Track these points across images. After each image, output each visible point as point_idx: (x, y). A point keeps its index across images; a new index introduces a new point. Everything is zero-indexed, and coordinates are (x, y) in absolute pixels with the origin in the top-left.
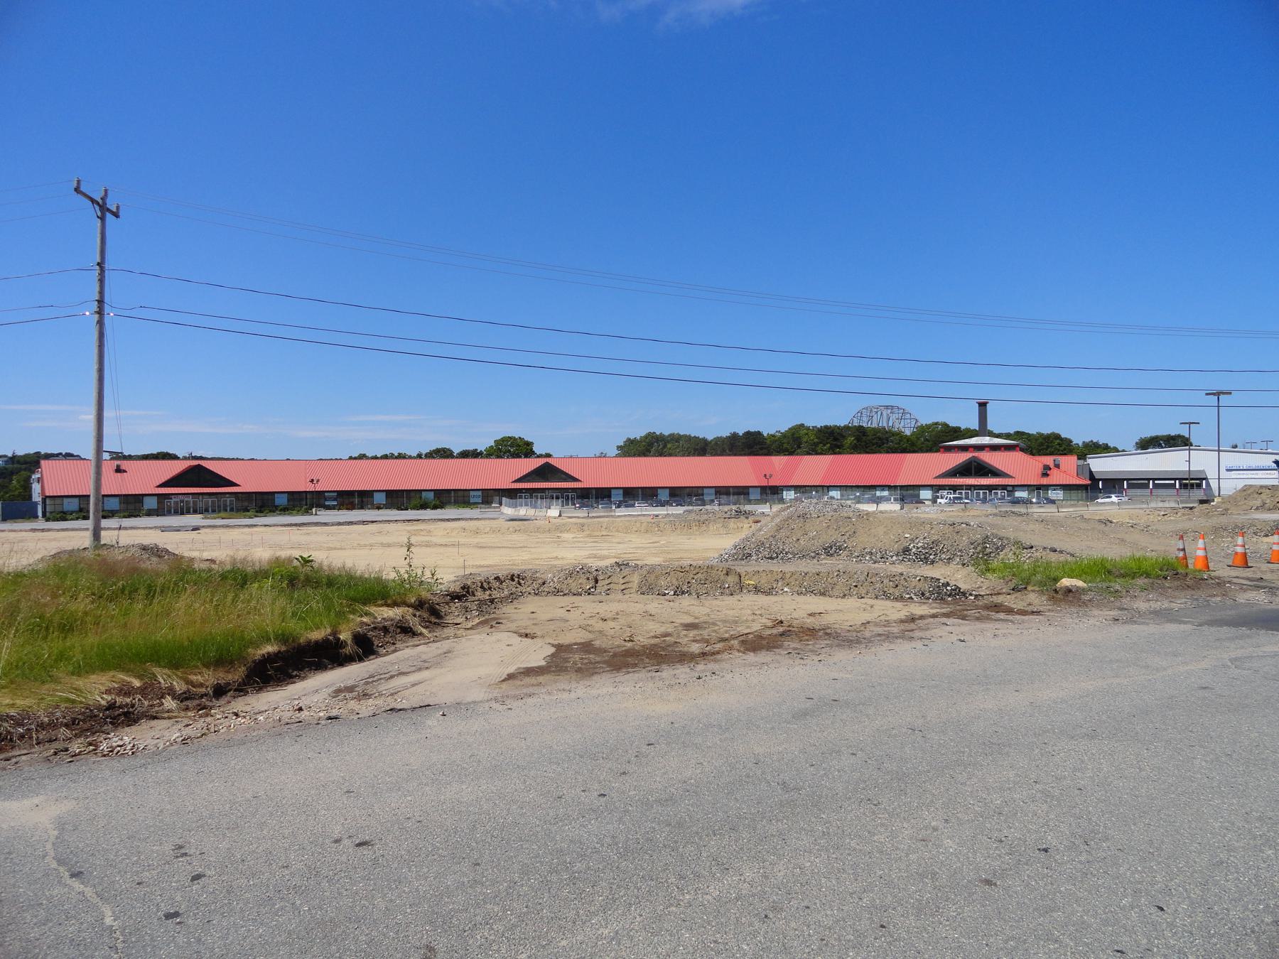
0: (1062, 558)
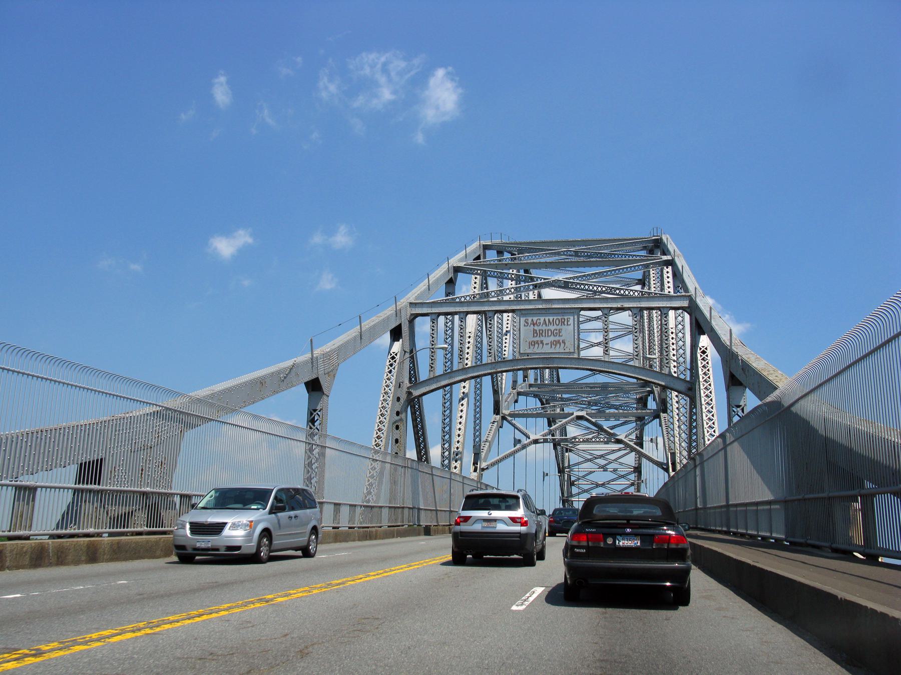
0: (666, 242)
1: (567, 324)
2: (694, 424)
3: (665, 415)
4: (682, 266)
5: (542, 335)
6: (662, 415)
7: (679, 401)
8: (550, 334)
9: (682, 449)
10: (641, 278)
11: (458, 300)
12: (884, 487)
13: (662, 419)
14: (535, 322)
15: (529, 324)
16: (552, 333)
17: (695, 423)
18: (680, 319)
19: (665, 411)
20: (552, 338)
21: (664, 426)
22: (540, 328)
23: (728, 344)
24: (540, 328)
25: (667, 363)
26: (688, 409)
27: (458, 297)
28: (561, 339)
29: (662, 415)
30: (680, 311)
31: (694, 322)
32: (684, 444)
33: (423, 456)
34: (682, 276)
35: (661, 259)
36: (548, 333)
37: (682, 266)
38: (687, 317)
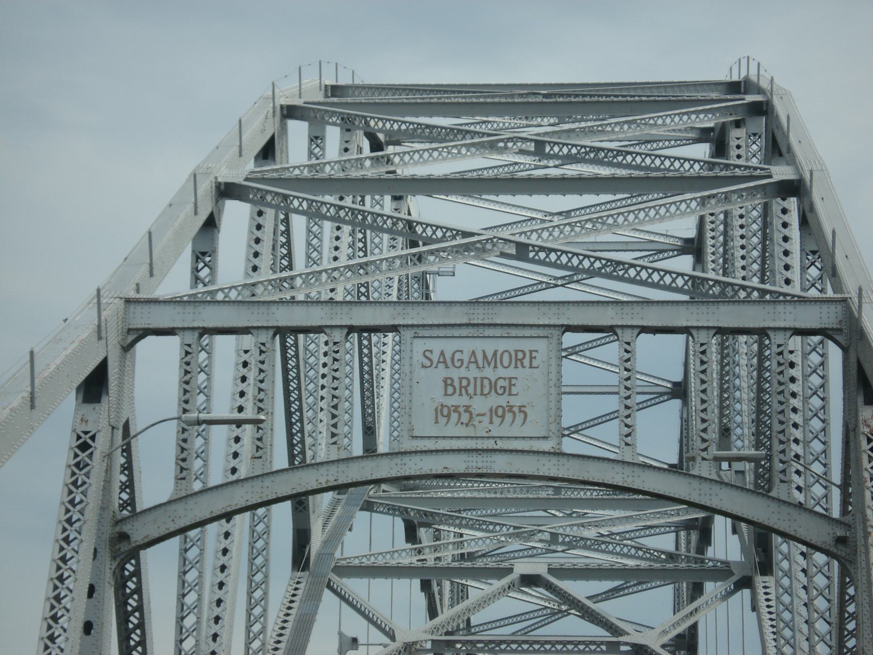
1: (531, 367)
2: (851, 626)
3: (770, 580)
4: (834, 233)
5: (467, 391)
6: (759, 580)
7: (811, 600)
8: (486, 391)
9: (816, 615)
10: (692, 234)
11: (220, 296)
12: (407, 248)
13: (761, 591)
14: (448, 356)
15: (435, 365)
16: (493, 386)
17: (854, 622)
18: (815, 358)
19: (766, 568)
20: (494, 401)
21: (764, 610)
22: (463, 372)
23: (388, 616)
24: (463, 372)
25: (628, 416)
26: (836, 601)
27: (222, 290)
28: (516, 402)
29: (759, 580)
30: (816, 339)
31: (854, 371)
32: (821, 626)
33: (133, 631)
34: (832, 255)
35: (770, 177)
36: (482, 386)
37: (834, 233)
38: (835, 354)
